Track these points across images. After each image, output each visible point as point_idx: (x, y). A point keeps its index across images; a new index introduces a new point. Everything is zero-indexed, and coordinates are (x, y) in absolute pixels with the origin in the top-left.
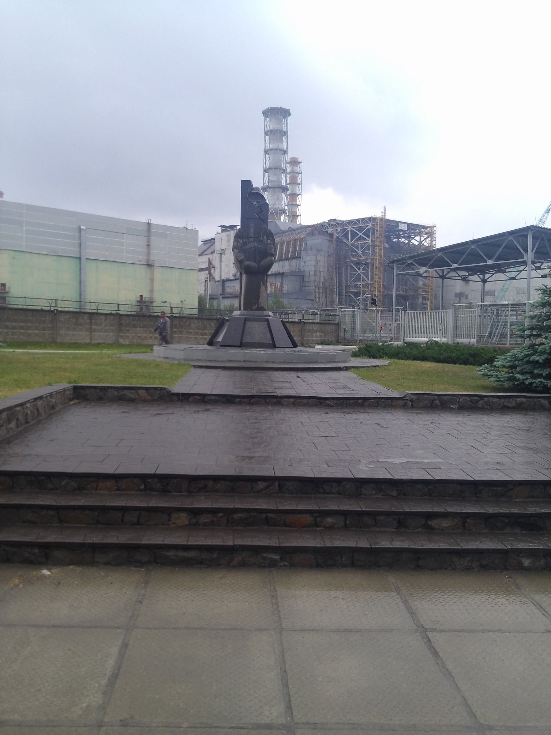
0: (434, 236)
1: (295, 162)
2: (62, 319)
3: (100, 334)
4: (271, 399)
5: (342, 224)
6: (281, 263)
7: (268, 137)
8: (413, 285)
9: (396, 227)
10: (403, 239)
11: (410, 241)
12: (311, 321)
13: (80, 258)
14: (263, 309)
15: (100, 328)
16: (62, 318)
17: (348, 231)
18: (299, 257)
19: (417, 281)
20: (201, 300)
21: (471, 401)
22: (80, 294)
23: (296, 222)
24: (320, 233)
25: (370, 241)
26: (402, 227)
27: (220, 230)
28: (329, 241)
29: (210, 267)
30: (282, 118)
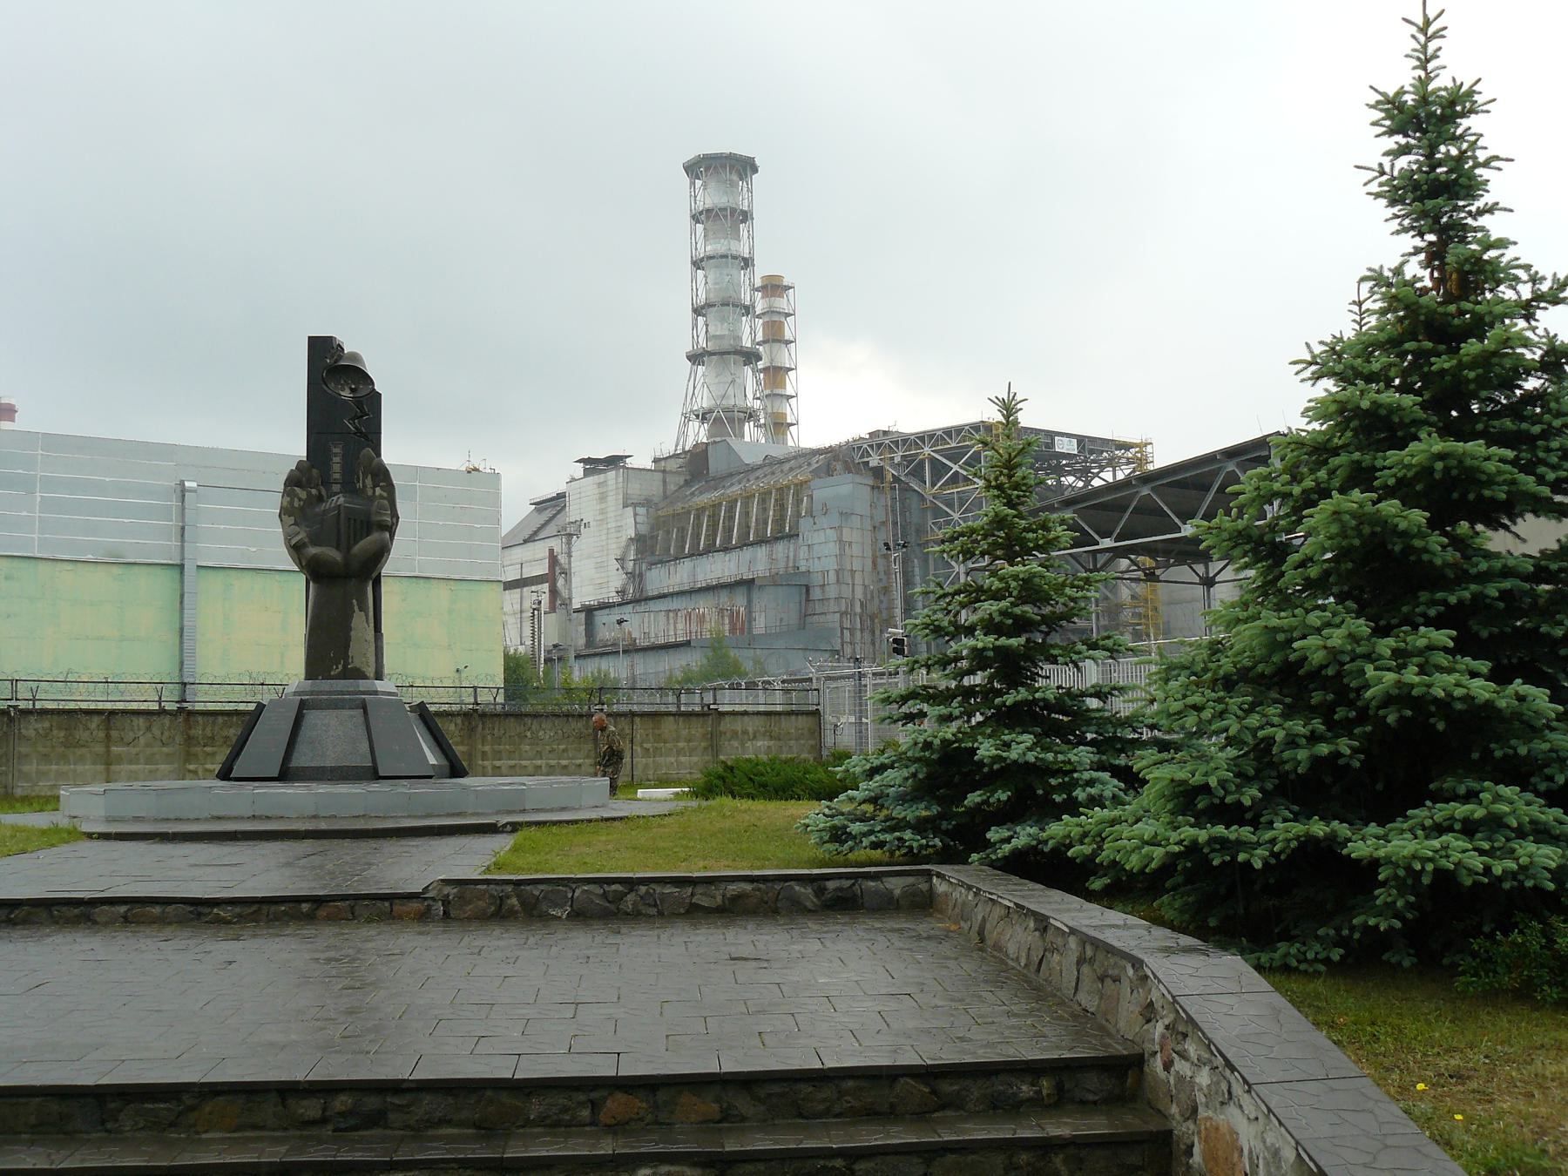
1: (774, 287)
2: (31, 733)
3: (134, 767)
4: (64, 909)
5: (905, 441)
6: (747, 553)
7: (700, 227)
8: (1107, 598)
10: (1071, 479)
11: (1088, 483)
12: (779, 708)
13: (182, 567)
14: (359, 674)
15: (134, 751)
16: (31, 728)
17: (922, 462)
18: (793, 535)
19: (1114, 589)
20: (514, 667)
21: (605, 895)
22: (182, 663)
23: (785, 442)
24: (850, 467)
26: (1065, 446)
27: (579, 470)
28: (873, 488)
29: (556, 570)
30: (735, 177)
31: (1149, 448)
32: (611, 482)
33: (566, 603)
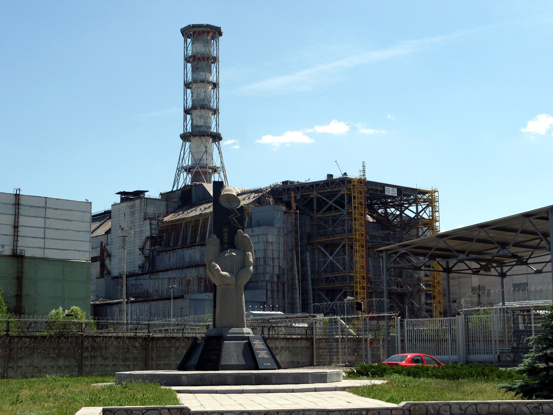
0: (437, 204)
9: (381, 191)
10: (393, 210)
11: (402, 212)
17: (312, 198)
25: (345, 212)
26: (390, 192)
27: (118, 199)
31: (436, 194)
32: (138, 206)
33: (109, 273)
